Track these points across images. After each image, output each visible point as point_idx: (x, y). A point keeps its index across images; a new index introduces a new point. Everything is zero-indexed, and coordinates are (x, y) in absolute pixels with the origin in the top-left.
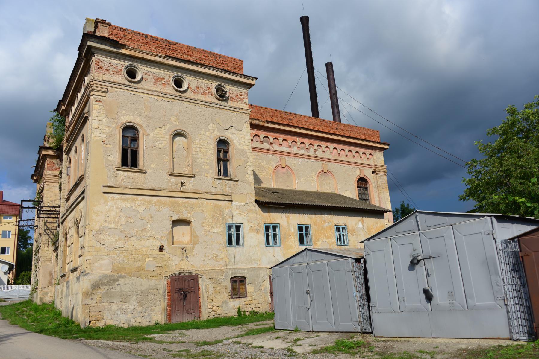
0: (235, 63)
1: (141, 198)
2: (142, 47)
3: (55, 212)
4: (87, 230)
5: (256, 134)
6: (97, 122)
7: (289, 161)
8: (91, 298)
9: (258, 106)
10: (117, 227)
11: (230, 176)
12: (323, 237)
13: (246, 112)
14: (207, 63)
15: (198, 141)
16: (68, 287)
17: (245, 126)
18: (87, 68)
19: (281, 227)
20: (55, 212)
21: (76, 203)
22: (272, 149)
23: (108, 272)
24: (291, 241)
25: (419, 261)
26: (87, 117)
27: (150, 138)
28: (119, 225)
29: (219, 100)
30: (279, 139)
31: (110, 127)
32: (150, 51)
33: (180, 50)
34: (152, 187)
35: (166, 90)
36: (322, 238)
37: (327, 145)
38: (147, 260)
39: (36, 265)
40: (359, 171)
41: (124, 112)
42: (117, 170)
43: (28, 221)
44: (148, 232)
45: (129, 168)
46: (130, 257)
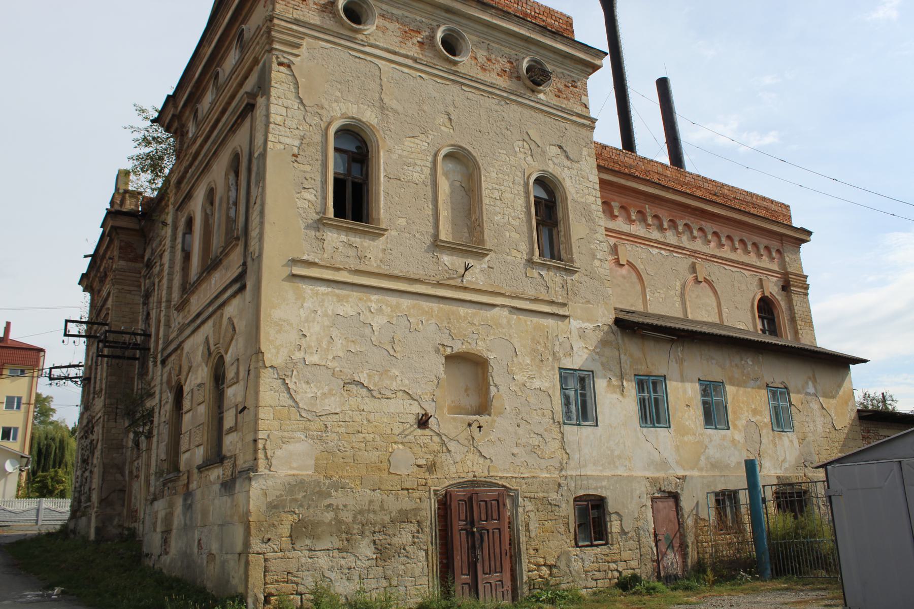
16: (188, 507)
21: (211, 309)
23: (308, 473)
27: (395, 157)
28: (330, 357)
30: (613, 203)
34: (401, 272)
36: (746, 414)
37: (702, 225)
39: (86, 457)
43: (69, 369)
45: (349, 223)
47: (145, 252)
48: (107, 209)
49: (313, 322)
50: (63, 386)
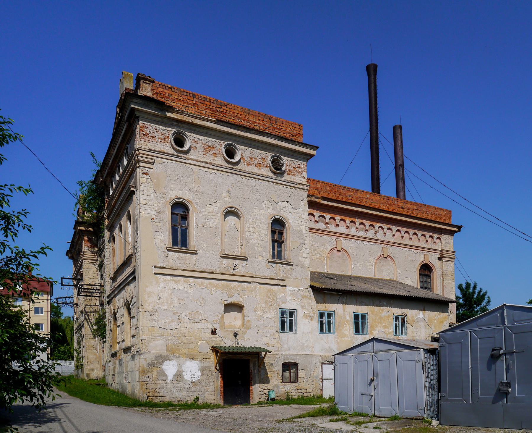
0: (294, 128)
1: (192, 280)
2: (190, 109)
3: (96, 291)
4: (141, 310)
5: (311, 212)
6: (146, 197)
7: (346, 243)
8: (148, 376)
9: (314, 180)
10: (169, 309)
11: (285, 259)
12: (380, 327)
13: (304, 187)
14: (262, 128)
15: (251, 220)
16: (120, 365)
17: (302, 204)
18: (129, 135)
19: (336, 315)
20: (96, 291)
22: (327, 230)
24: (346, 329)
25: (501, 355)
26: (134, 191)
27: (200, 215)
28: (172, 306)
29: (274, 173)
30: (336, 218)
31: (159, 203)
32: (199, 114)
33: (231, 113)
34: (204, 269)
35: (217, 161)
36: (379, 328)
38: (200, 342)
40: (423, 256)
41: (172, 186)
42: (168, 250)
43: (66, 299)
44: (200, 314)
46: (184, 339)
47: (98, 242)
48: (75, 221)
49: (164, 292)
50: (64, 307)
